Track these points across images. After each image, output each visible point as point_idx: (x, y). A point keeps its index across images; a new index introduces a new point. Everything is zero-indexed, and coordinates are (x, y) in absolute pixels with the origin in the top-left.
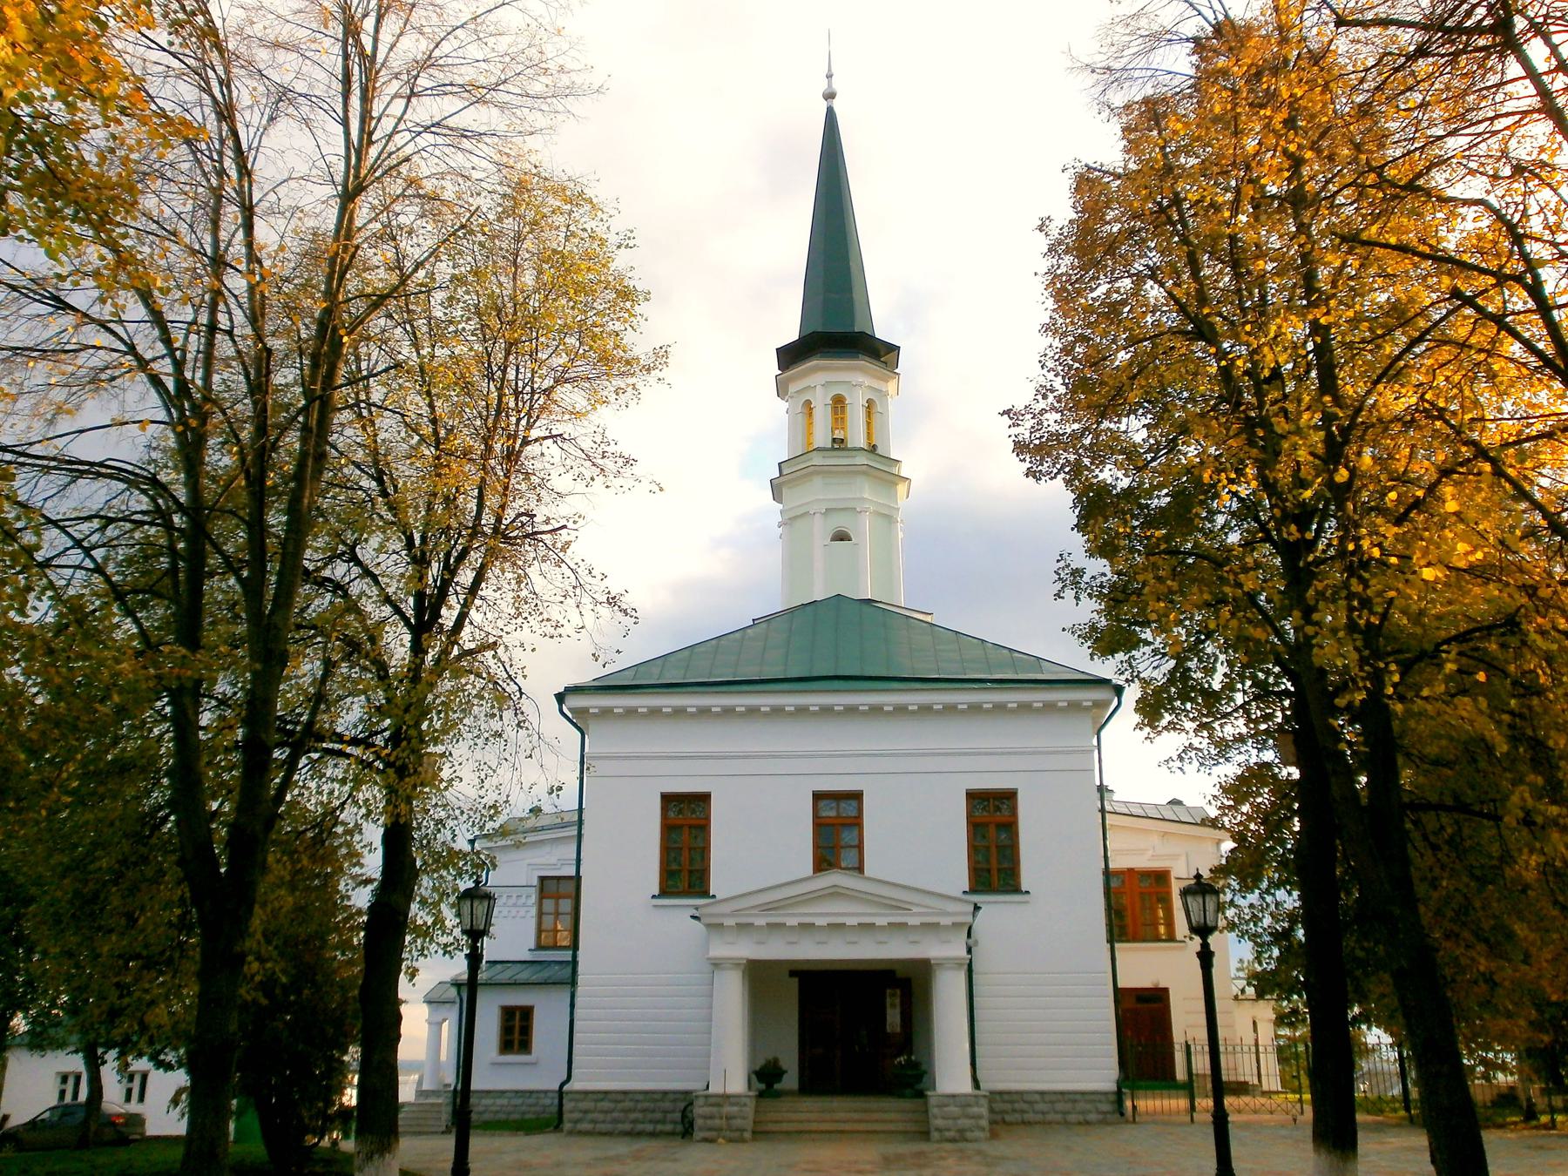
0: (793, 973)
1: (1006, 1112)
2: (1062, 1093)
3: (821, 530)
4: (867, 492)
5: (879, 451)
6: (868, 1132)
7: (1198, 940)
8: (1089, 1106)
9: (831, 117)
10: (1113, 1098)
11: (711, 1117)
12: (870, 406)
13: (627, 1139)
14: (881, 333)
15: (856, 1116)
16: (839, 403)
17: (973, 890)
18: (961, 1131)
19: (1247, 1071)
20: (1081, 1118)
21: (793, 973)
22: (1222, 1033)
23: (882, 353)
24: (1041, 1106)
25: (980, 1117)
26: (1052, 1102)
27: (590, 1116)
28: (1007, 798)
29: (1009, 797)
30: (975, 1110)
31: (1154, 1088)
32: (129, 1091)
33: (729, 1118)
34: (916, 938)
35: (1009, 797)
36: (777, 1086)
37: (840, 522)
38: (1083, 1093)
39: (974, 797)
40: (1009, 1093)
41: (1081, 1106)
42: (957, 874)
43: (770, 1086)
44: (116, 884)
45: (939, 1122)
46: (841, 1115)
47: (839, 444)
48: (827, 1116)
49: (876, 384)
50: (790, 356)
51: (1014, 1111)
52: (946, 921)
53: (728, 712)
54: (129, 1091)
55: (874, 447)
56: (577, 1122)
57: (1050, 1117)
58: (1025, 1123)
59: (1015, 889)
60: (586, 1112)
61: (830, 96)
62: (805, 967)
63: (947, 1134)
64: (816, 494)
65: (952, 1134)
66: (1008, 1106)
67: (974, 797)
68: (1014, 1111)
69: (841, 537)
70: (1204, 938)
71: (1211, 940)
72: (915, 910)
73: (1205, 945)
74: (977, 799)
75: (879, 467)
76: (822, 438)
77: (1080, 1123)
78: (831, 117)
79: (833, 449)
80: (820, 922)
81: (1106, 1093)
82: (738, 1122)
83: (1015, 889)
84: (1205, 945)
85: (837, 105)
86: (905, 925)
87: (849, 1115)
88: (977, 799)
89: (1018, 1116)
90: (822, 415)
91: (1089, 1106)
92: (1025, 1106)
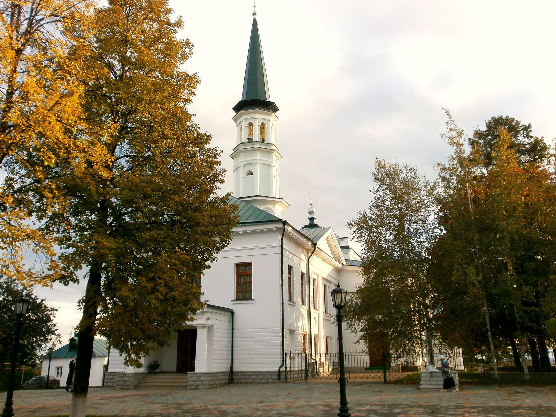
1: (241, 379)
2: (261, 372)
3: (243, 172)
4: (259, 157)
5: (266, 141)
6: (172, 386)
8: (269, 377)
9: (255, 21)
10: (277, 373)
11: (120, 381)
12: (263, 124)
13: (399, 387)
16: (251, 125)
17: (238, 299)
18: (197, 386)
20: (266, 381)
22: (344, 348)
23: (271, 107)
24: (254, 377)
25: (204, 381)
26: (257, 375)
27: (112, 381)
29: (249, 265)
31: (376, 369)
32: (58, 373)
33: (125, 381)
35: (249, 265)
36: (157, 370)
37: (250, 168)
38: (254, 372)
39: (238, 265)
40: (243, 372)
41: (267, 376)
42: (232, 294)
43: (154, 370)
45: (190, 383)
46: (170, 380)
47: (250, 141)
49: (264, 117)
50: (239, 108)
51: (244, 378)
54: (58, 373)
55: (263, 140)
56: (108, 382)
57: (255, 381)
58: (241, 383)
59: (250, 298)
60: (111, 379)
61: (255, 14)
63: (192, 387)
64: (243, 159)
66: (242, 377)
67: (238, 265)
68: (244, 378)
69: (251, 173)
74: (238, 266)
75: (266, 147)
76: (245, 140)
77: (266, 383)
78: (255, 21)
79: (249, 142)
81: (275, 372)
82: (128, 383)
83: (250, 298)
85: (256, 17)
88: (238, 266)
89: (245, 381)
90: (246, 131)
91: (269, 377)
92: (248, 377)
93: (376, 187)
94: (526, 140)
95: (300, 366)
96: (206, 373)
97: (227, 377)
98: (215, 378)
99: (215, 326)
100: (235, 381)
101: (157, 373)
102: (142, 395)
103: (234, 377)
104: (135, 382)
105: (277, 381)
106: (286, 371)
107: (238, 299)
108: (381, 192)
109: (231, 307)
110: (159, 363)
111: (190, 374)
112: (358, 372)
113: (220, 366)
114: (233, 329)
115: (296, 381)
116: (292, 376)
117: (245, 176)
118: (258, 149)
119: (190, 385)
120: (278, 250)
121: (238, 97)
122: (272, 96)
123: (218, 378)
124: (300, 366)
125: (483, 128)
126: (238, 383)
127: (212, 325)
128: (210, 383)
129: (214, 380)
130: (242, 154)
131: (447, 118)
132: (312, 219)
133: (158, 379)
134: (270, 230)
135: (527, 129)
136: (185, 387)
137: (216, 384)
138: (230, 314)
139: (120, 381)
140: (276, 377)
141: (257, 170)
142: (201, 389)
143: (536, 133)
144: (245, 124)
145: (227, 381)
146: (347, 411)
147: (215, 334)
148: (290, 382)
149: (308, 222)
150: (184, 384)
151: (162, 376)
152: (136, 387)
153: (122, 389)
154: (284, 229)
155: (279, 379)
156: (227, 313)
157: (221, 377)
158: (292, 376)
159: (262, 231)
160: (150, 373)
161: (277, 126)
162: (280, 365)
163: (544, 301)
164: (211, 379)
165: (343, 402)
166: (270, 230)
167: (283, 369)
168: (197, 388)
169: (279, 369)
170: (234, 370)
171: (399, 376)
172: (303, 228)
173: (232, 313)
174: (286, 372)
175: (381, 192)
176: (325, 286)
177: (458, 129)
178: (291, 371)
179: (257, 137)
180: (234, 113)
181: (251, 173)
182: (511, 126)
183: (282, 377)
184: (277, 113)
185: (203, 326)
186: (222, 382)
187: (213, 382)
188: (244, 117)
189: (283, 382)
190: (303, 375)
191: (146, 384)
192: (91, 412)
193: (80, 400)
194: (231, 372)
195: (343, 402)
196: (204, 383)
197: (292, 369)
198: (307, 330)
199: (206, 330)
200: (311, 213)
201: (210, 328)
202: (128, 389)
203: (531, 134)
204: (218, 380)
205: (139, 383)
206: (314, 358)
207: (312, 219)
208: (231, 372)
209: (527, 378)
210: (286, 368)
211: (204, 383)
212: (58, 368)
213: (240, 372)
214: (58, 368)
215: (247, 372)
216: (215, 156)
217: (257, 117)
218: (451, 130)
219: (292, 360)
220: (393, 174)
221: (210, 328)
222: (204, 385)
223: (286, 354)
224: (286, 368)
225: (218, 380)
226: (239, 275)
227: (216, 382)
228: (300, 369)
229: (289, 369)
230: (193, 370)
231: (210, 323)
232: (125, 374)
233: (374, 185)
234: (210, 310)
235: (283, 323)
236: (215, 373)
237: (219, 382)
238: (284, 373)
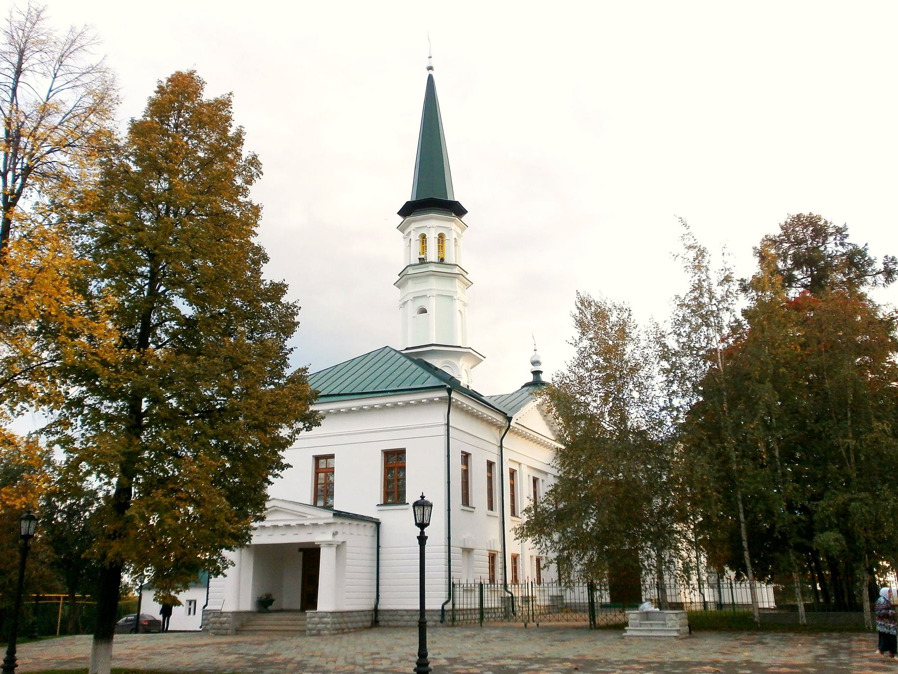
0: (300, 550)
3: (412, 308)
4: (435, 285)
5: (446, 261)
6: (285, 631)
7: (419, 530)
9: (430, 79)
10: (440, 613)
11: (215, 623)
12: (441, 236)
14: (457, 198)
15: (289, 622)
16: (423, 237)
18: (319, 631)
19: (766, 599)
21: (300, 550)
23: (457, 210)
25: (328, 623)
28: (401, 453)
30: (326, 619)
32: (190, 609)
33: (221, 623)
34: (310, 531)
35: (401, 453)
36: (270, 608)
37: (421, 303)
38: (407, 611)
40: (392, 611)
42: (378, 497)
43: (266, 607)
44: (29, 509)
45: (310, 626)
47: (422, 261)
48: (279, 623)
50: (408, 210)
52: (320, 522)
53: (395, 406)
54: (190, 609)
55: (442, 260)
58: (389, 627)
62: (307, 547)
64: (412, 288)
65: (314, 632)
66: (391, 618)
69: (423, 311)
70: (422, 529)
71: (425, 530)
72: (309, 517)
73: (422, 533)
74: (388, 454)
78: (430, 79)
80: (281, 524)
81: (438, 611)
84: (422, 533)
86: (316, 524)
87: (276, 622)
88: (388, 454)
89: (395, 623)
90: (416, 246)
93: (577, 338)
94: (840, 248)
95: (473, 602)
96: (331, 613)
97: (369, 618)
98: (346, 619)
99: (348, 544)
100: (381, 623)
101: (270, 612)
102: (230, 644)
103: (380, 618)
104: (237, 624)
105: (439, 623)
106: (453, 609)
107: (386, 503)
108: (586, 343)
109: (375, 515)
110: (274, 597)
111: (309, 613)
112: (580, 610)
113: (358, 600)
114: (378, 547)
115: (467, 625)
116: (466, 617)
117: (415, 314)
118: (434, 274)
119: (310, 630)
120: (443, 430)
121: (407, 194)
122: (458, 193)
123: (352, 619)
124: (473, 602)
125: (777, 232)
126: (385, 626)
127: (344, 542)
128: (338, 626)
129: (346, 623)
130: (410, 282)
131: (684, 230)
132: (537, 373)
133: (270, 621)
134: (431, 401)
135: (840, 232)
136: (302, 633)
137: (349, 628)
138: (374, 525)
139: (215, 623)
140: (438, 618)
141: (432, 305)
142: (325, 635)
143: (856, 238)
144: (415, 236)
145: (369, 624)
146: (427, 664)
147: (348, 555)
148: (458, 626)
149: (530, 378)
150: (301, 628)
151: (275, 616)
152: (238, 631)
153: (217, 634)
154: (450, 399)
155: (442, 622)
156: (369, 525)
157: (358, 618)
158: (466, 617)
159: (395, 406)
160: (259, 612)
161: (464, 242)
162: (444, 600)
163: (817, 505)
164: (341, 620)
165: (422, 653)
166: (431, 401)
167: (449, 606)
168: (318, 634)
169: (443, 607)
170: (380, 607)
171: (611, 617)
172: (523, 387)
173: (378, 524)
174: (453, 609)
175: (586, 343)
176: (535, 480)
177: (698, 245)
178: (460, 610)
179: (432, 255)
180: (400, 219)
181: (423, 311)
182: (820, 231)
183: (447, 618)
184: (465, 218)
185: (329, 544)
186: (360, 624)
187: (343, 626)
188: (413, 226)
189: (448, 626)
190: (478, 616)
191: (255, 627)
192: (116, 665)
193: (102, 648)
194: (376, 610)
195: (422, 653)
196: (329, 626)
197: (461, 607)
198: (498, 548)
199: (334, 549)
200: (535, 363)
201: (340, 547)
202: (226, 634)
203: (846, 241)
204: (352, 622)
205: (242, 625)
206: (509, 590)
207: (537, 373)
208: (376, 610)
209: (803, 620)
210: (453, 605)
211: (329, 626)
212: (190, 602)
213: (388, 611)
214: (190, 602)
215: (397, 611)
216: (294, 314)
217: (432, 224)
218: (690, 247)
219: (465, 594)
220: (601, 315)
221: (340, 547)
222: (328, 629)
223: (454, 585)
224: (453, 605)
225: (352, 622)
226: (388, 469)
227: (350, 625)
228: (473, 607)
229: (457, 607)
230: (315, 608)
231: (339, 539)
232: (222, 613)
233: (576, 333)
234: (339, 521)
235: (449, 538)
236: (347, 612)
237: (354, 625)
238: (450, 613)
